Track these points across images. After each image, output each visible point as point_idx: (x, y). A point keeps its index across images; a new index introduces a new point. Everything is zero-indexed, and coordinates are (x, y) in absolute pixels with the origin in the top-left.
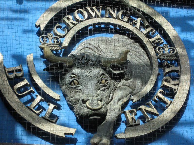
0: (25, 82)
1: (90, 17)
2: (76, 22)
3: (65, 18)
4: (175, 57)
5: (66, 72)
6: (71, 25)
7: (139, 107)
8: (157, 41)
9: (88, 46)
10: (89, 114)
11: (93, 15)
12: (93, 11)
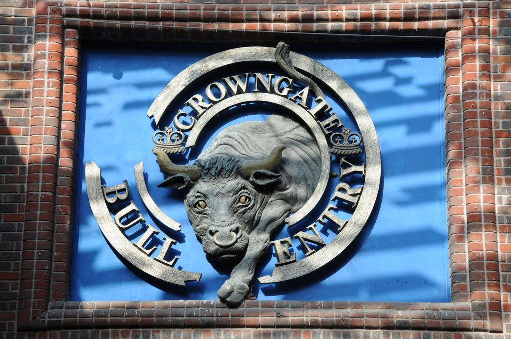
0: (132, 207)
1: (230, 93)
2: (207, 105)
3: (191, 99)
4: (359, 149)
5: (190, 187)
6: (200, 111)
7: (295, 235)
8: (332, 125)
9: (226, 140)
10: (218, 252)
11: (235, 90)
12: (235, 82)
